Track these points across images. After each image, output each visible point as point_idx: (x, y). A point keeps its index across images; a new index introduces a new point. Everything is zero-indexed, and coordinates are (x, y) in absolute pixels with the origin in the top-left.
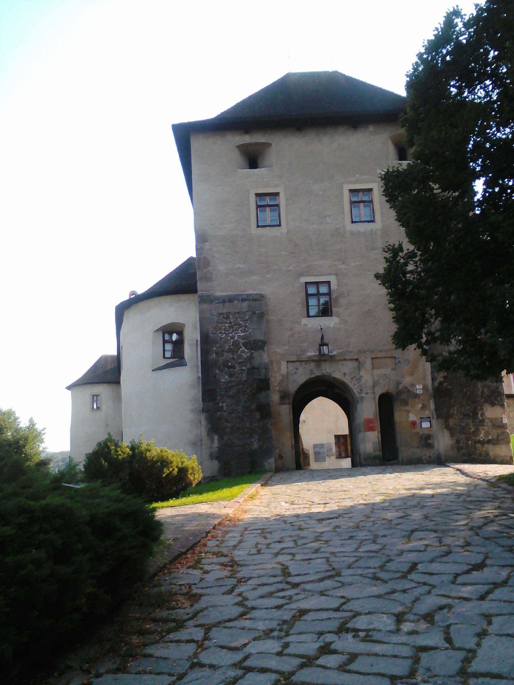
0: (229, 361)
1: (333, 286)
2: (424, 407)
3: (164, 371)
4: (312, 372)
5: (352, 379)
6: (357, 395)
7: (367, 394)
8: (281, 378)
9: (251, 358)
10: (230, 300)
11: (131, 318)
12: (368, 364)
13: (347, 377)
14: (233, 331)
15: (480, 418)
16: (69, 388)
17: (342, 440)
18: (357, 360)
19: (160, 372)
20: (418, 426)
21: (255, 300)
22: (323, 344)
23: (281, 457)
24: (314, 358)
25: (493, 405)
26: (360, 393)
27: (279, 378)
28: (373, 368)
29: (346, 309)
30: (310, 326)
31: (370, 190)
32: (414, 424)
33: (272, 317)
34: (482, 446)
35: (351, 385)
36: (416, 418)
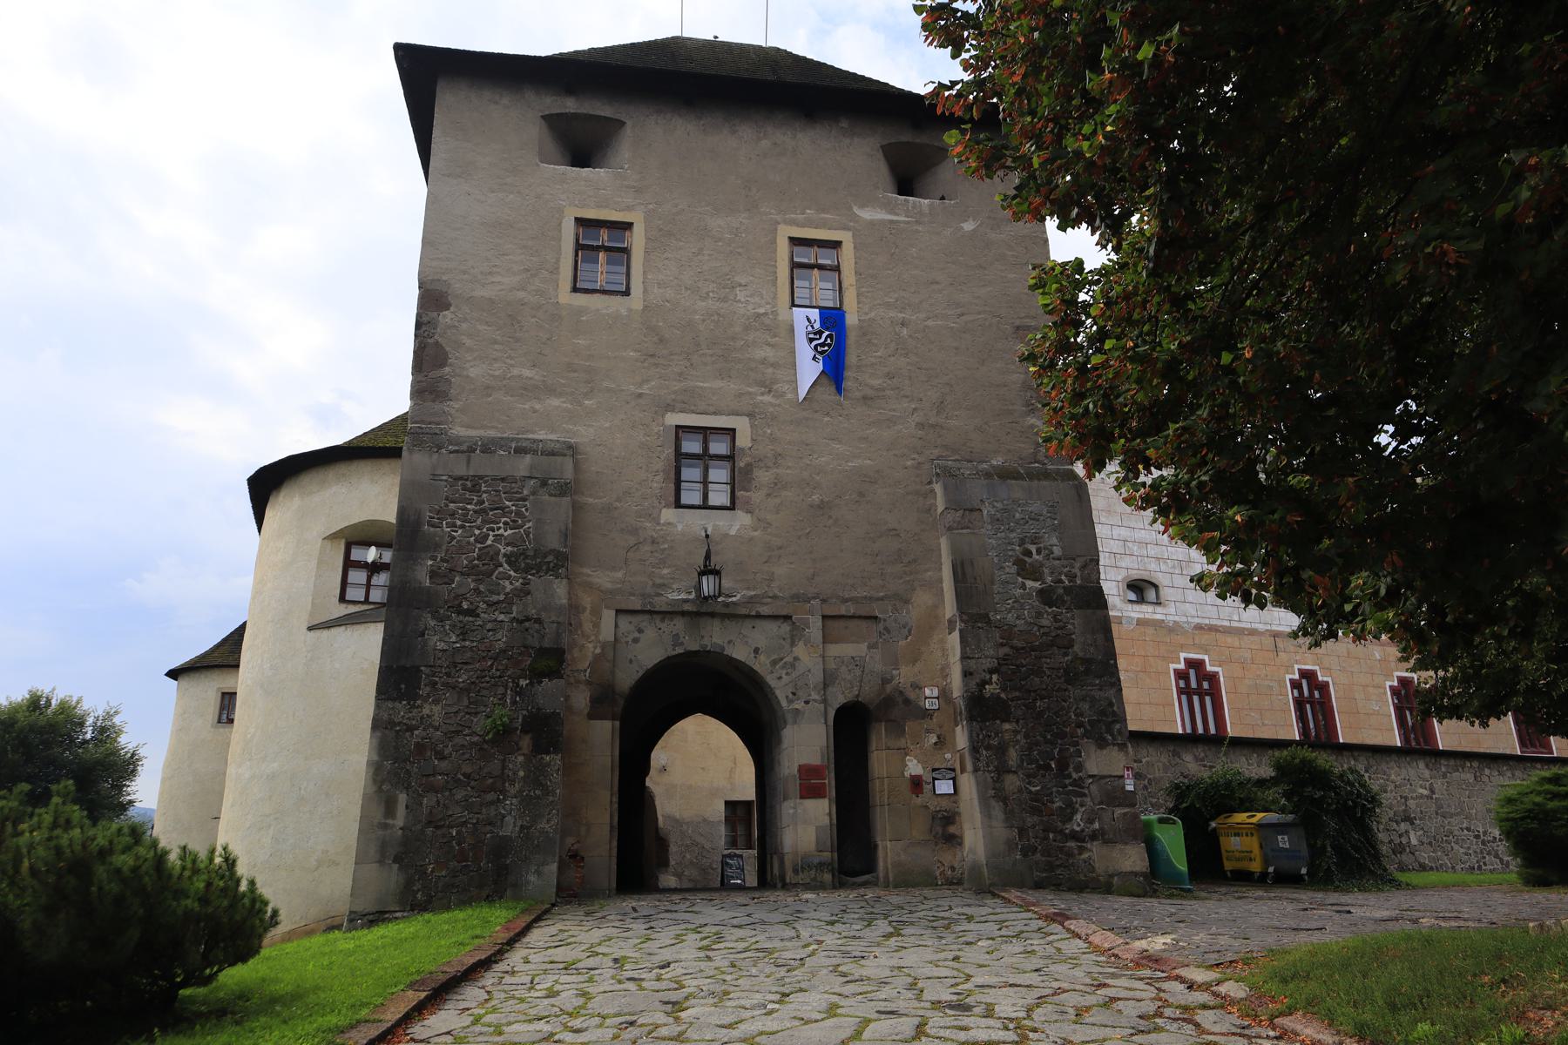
0: (463, 597)
1: (743, 441)
2: (941, 743)
3: (334, 631)
4: (676, 640)
5: (774, 663)
6: (784, 704)
7: (807, 702)
8: (598, 651)
9: (524, 592)
10: (488, 447)
11: (282, 508)
12: (816, 623)
13: (762, 658)
14: (484, 522)
15: (1075, 776)
16: (173, 674)
17: (740, 812)
18: (787, 618)
19: (325, 634)
20: (927, 788)
21: (553, 454)
22: (708, 570)
23: (575, 856)
24: (687, 607)
25: (1102, 744)
26: (790, 702)
27: (592, 649)
28: (826, 639)
29: (768, 495)
30: (680, 527)
31: (836, 245)
32: (916, 784)
33: (590, 500)
34: (1082, 850)
35: (771, 680)
36: (933, 768)
